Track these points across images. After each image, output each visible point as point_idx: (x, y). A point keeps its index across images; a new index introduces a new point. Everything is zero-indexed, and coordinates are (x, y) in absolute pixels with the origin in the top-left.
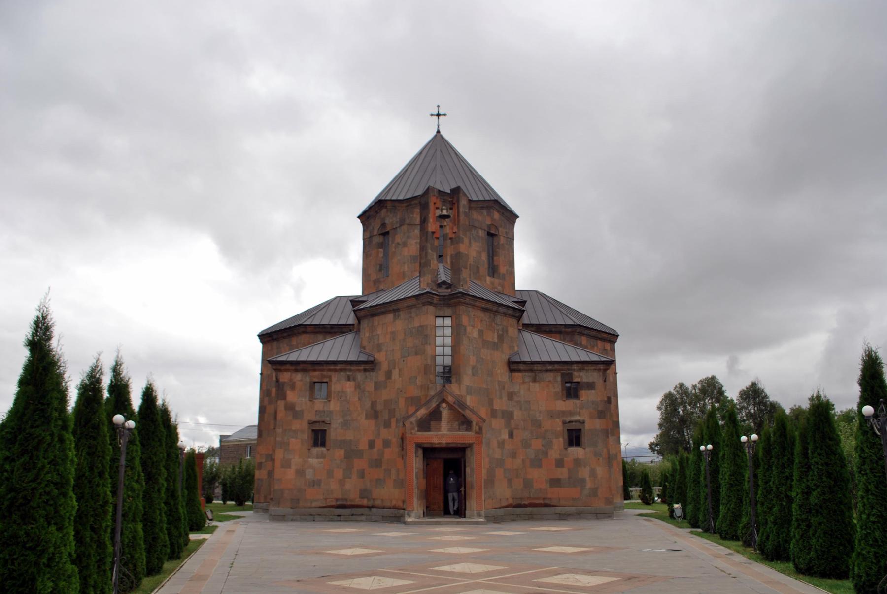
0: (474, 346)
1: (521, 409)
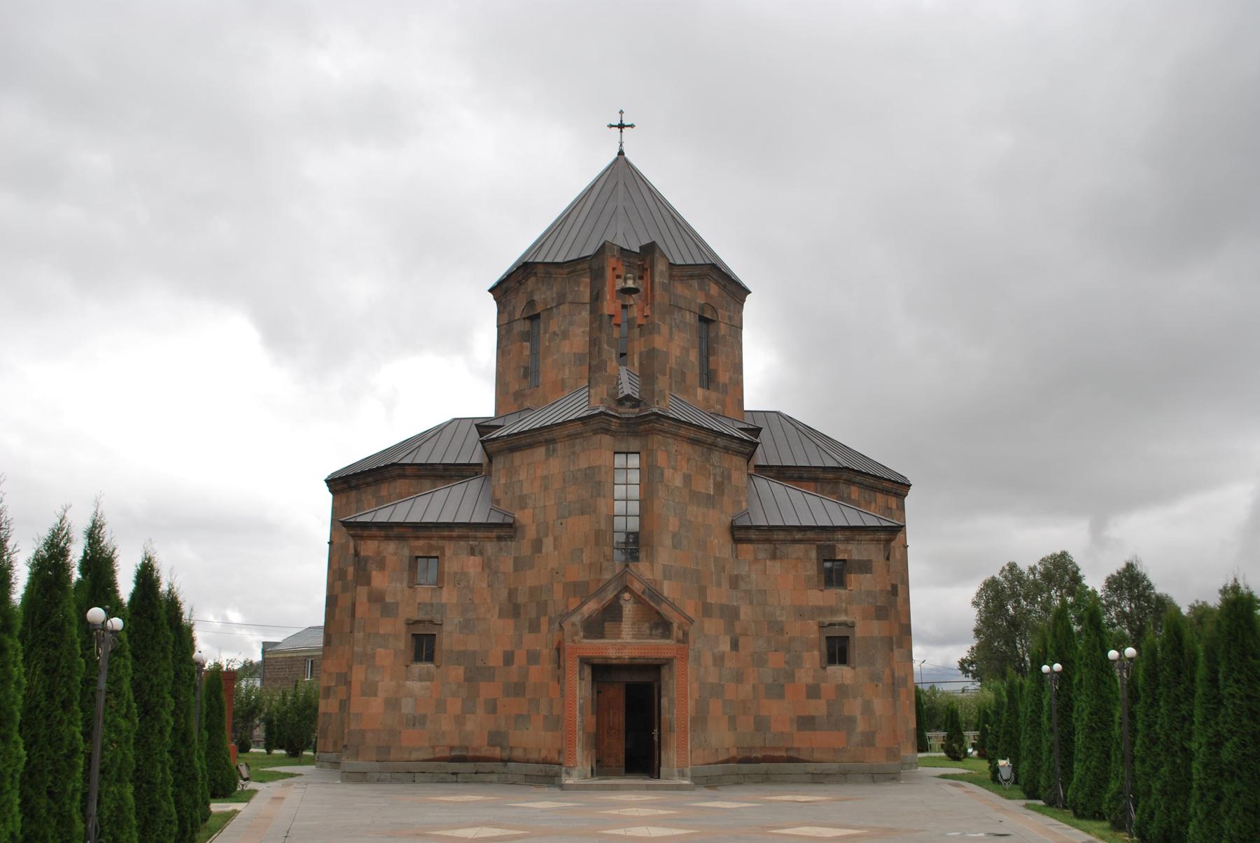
0: (677, 500)
1: (751, 603)
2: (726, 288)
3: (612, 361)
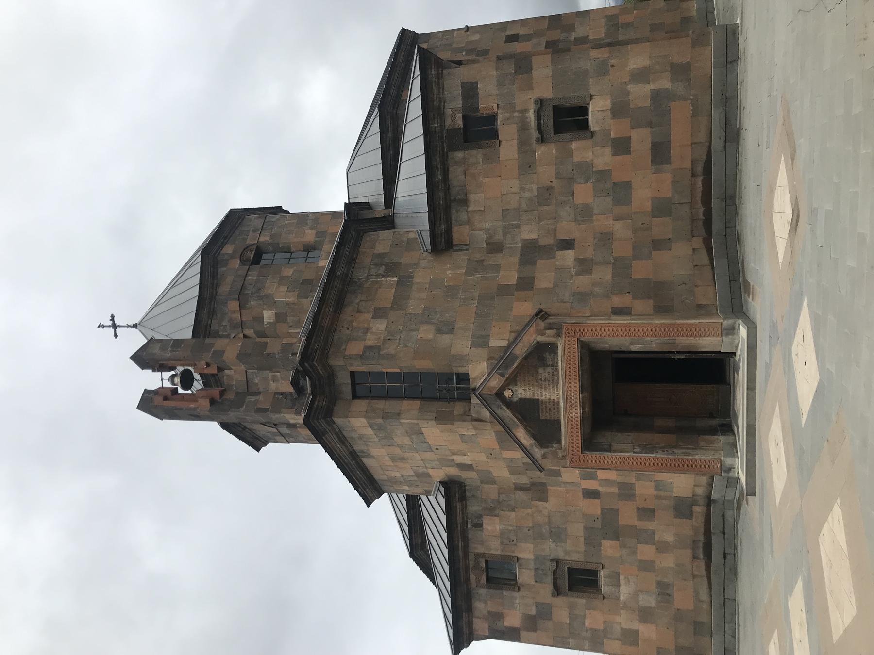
1: (518, 226)
2: (226, 237)
3: (258, 400)
